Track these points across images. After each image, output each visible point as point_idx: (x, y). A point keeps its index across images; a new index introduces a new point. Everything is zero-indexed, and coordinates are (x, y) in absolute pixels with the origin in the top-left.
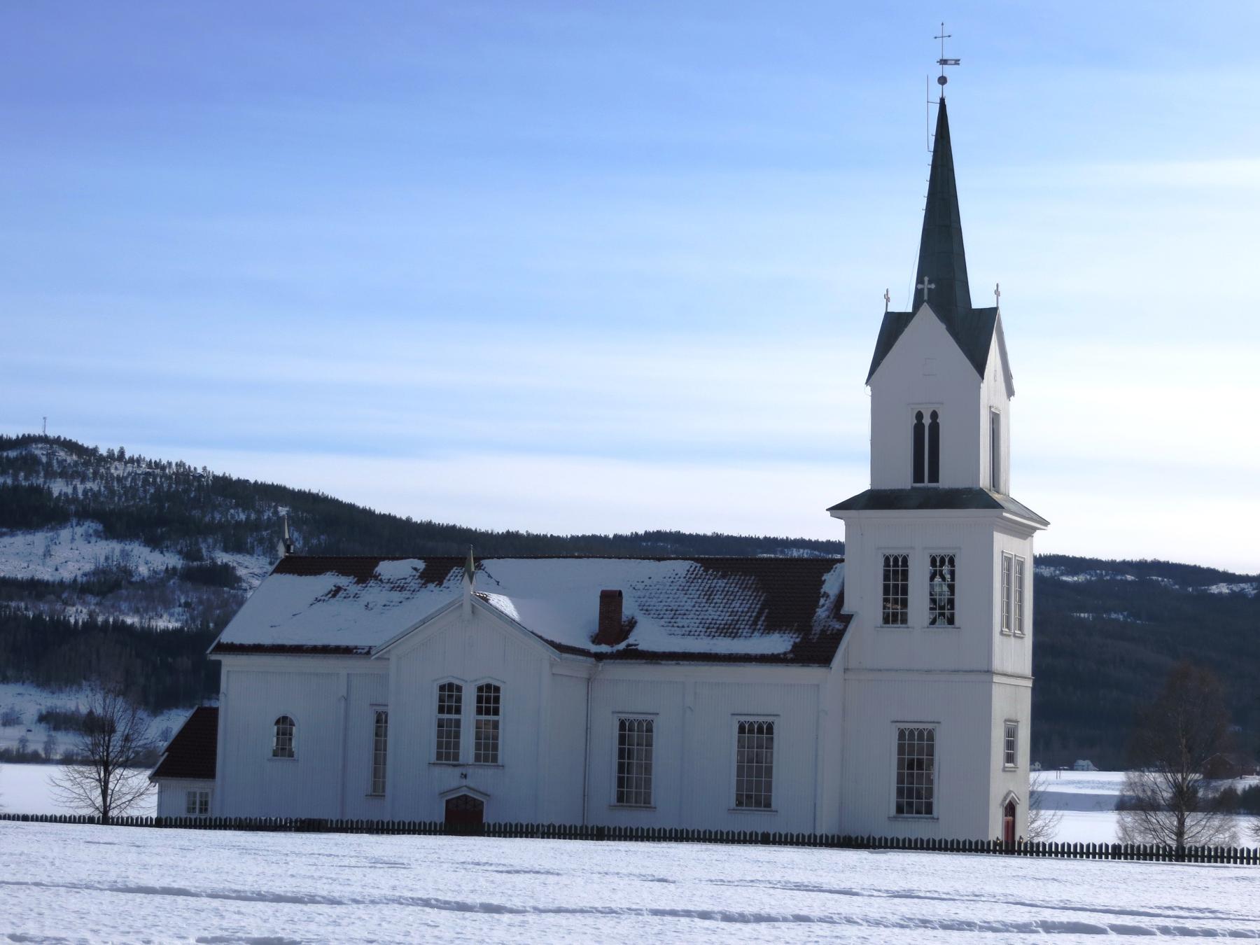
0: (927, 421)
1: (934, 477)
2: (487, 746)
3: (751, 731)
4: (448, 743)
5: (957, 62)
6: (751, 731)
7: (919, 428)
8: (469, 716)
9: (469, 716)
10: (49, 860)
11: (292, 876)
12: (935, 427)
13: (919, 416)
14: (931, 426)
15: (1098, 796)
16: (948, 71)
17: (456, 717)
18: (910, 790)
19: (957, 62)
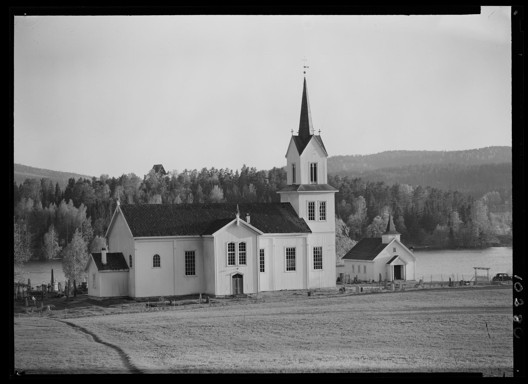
0: (313, 166)
1: (315, 180)
2: (157, 262)
3: (189, 254)
4: (157, 262)
5: (308, 67)
6: (189, 254)
7: (312, 168)
8: (237, 252)
9: (237, 252)
10: (25, 362)
11: (229, 358)
12: (315, 168)
13: (311, 165)
14: (314, 167)
15: (404, 245)
16: (306, 70)
17: (244, 252)
18: (191, 258)
19: (308, 67)
